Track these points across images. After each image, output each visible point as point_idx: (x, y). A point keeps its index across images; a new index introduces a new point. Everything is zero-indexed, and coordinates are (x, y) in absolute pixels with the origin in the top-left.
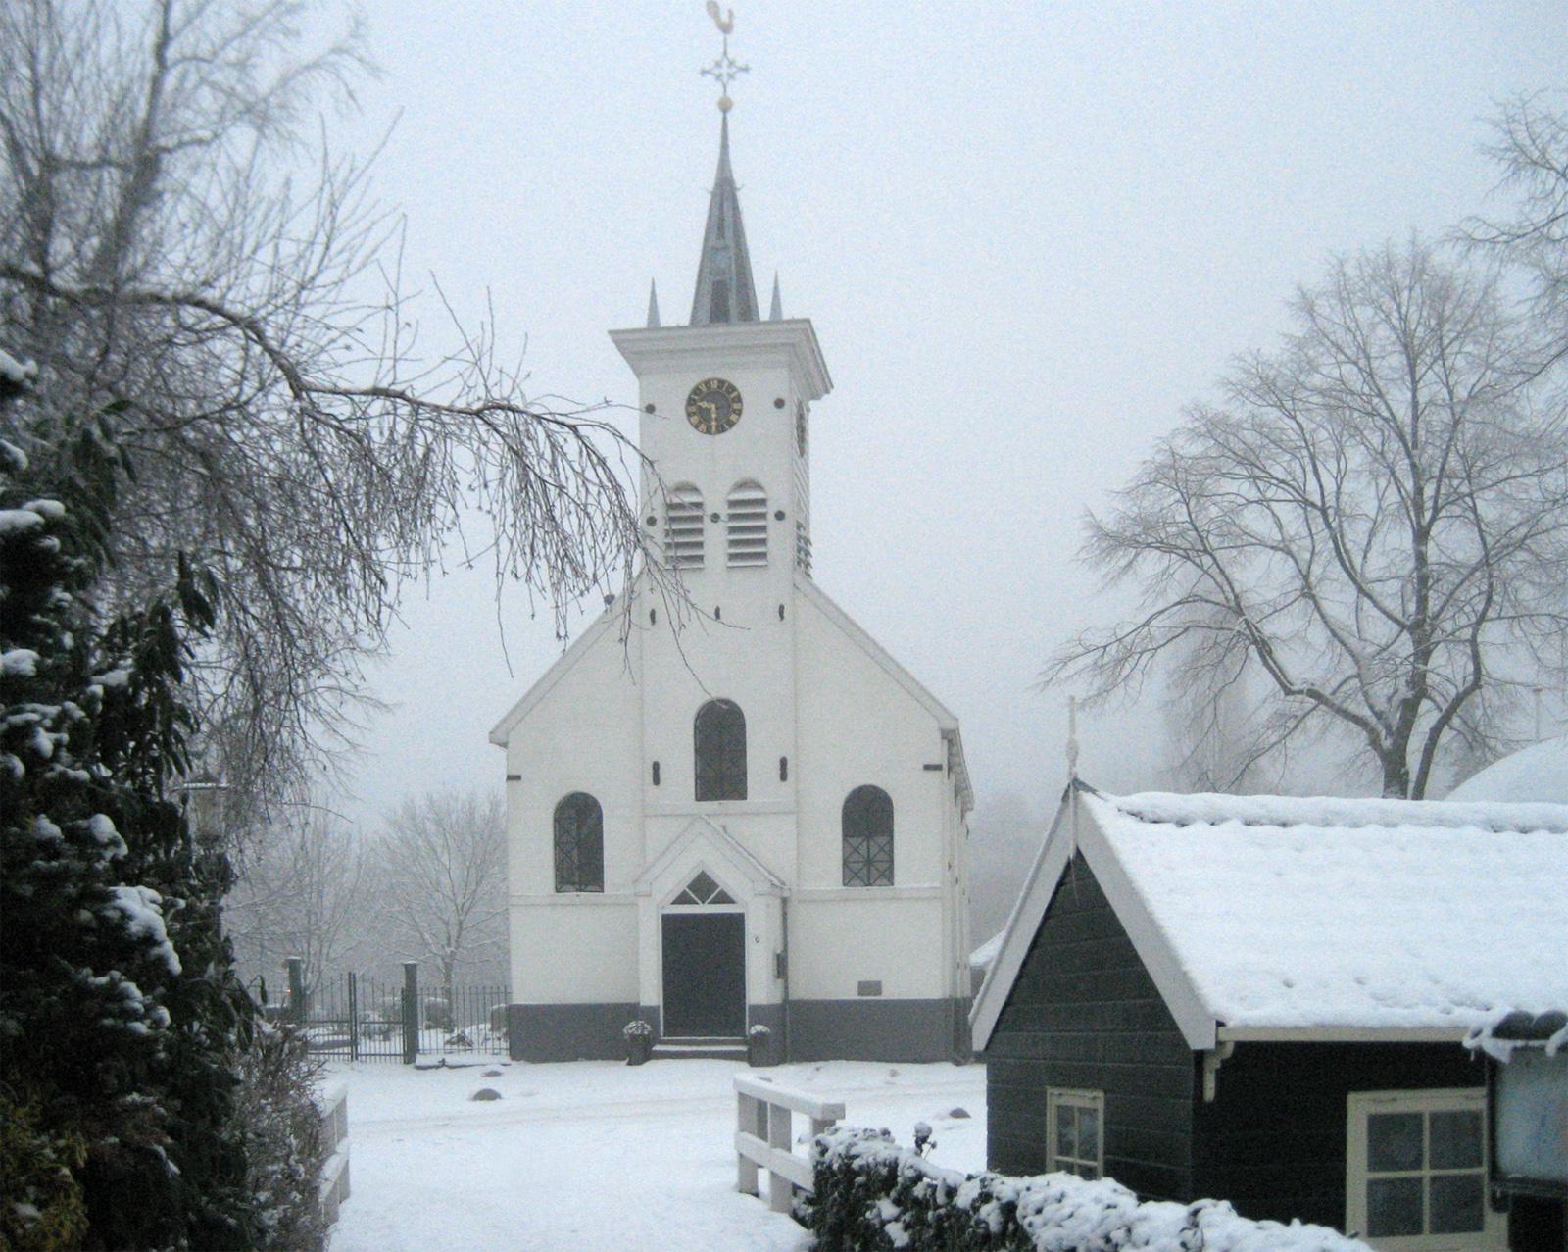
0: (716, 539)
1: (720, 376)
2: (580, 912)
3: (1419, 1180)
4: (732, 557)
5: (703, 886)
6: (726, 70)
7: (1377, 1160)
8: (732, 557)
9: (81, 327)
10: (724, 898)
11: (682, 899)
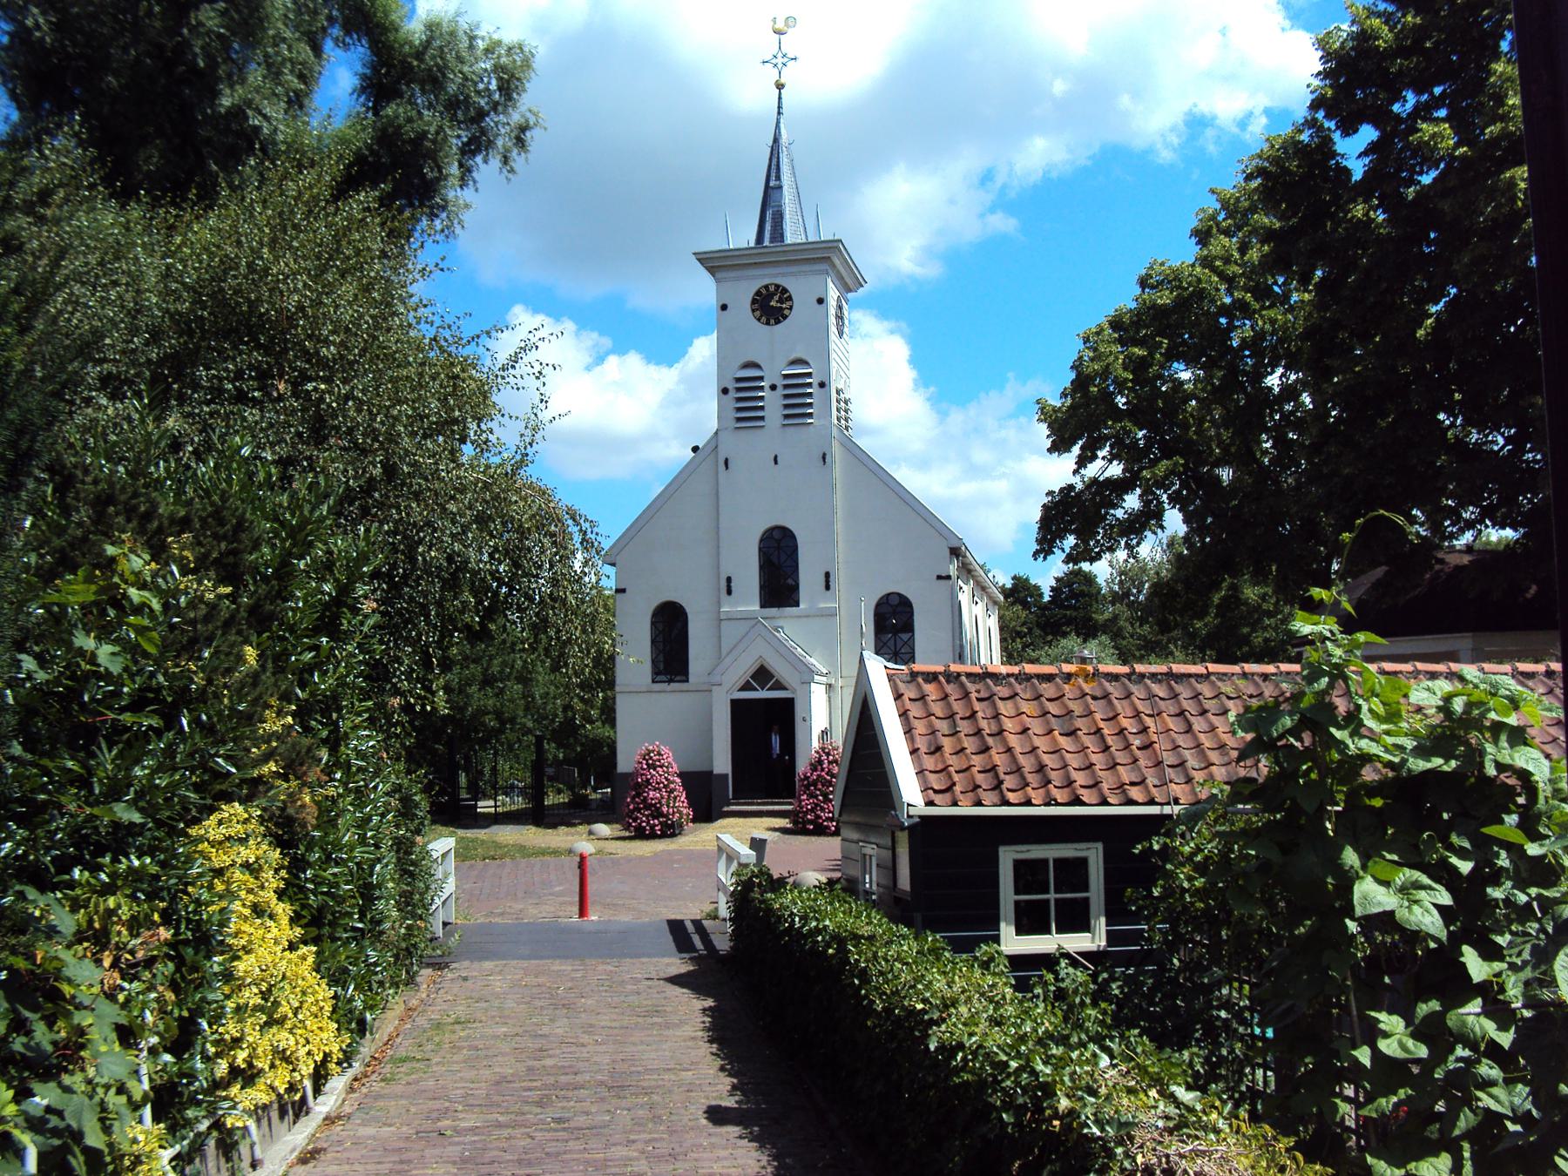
0: (773, 404)
1: (778, 281)
2: (672, 701)
3: (1047, 901)
4: (787, 417)
5: (762, 675)
6: (780, 60)
7: (1060, 863)
8: (787, 417)
9: (1535, 461)
10: (779, 686)
11: (746, 687)
